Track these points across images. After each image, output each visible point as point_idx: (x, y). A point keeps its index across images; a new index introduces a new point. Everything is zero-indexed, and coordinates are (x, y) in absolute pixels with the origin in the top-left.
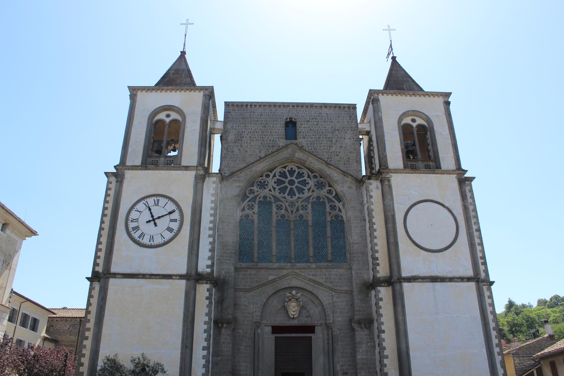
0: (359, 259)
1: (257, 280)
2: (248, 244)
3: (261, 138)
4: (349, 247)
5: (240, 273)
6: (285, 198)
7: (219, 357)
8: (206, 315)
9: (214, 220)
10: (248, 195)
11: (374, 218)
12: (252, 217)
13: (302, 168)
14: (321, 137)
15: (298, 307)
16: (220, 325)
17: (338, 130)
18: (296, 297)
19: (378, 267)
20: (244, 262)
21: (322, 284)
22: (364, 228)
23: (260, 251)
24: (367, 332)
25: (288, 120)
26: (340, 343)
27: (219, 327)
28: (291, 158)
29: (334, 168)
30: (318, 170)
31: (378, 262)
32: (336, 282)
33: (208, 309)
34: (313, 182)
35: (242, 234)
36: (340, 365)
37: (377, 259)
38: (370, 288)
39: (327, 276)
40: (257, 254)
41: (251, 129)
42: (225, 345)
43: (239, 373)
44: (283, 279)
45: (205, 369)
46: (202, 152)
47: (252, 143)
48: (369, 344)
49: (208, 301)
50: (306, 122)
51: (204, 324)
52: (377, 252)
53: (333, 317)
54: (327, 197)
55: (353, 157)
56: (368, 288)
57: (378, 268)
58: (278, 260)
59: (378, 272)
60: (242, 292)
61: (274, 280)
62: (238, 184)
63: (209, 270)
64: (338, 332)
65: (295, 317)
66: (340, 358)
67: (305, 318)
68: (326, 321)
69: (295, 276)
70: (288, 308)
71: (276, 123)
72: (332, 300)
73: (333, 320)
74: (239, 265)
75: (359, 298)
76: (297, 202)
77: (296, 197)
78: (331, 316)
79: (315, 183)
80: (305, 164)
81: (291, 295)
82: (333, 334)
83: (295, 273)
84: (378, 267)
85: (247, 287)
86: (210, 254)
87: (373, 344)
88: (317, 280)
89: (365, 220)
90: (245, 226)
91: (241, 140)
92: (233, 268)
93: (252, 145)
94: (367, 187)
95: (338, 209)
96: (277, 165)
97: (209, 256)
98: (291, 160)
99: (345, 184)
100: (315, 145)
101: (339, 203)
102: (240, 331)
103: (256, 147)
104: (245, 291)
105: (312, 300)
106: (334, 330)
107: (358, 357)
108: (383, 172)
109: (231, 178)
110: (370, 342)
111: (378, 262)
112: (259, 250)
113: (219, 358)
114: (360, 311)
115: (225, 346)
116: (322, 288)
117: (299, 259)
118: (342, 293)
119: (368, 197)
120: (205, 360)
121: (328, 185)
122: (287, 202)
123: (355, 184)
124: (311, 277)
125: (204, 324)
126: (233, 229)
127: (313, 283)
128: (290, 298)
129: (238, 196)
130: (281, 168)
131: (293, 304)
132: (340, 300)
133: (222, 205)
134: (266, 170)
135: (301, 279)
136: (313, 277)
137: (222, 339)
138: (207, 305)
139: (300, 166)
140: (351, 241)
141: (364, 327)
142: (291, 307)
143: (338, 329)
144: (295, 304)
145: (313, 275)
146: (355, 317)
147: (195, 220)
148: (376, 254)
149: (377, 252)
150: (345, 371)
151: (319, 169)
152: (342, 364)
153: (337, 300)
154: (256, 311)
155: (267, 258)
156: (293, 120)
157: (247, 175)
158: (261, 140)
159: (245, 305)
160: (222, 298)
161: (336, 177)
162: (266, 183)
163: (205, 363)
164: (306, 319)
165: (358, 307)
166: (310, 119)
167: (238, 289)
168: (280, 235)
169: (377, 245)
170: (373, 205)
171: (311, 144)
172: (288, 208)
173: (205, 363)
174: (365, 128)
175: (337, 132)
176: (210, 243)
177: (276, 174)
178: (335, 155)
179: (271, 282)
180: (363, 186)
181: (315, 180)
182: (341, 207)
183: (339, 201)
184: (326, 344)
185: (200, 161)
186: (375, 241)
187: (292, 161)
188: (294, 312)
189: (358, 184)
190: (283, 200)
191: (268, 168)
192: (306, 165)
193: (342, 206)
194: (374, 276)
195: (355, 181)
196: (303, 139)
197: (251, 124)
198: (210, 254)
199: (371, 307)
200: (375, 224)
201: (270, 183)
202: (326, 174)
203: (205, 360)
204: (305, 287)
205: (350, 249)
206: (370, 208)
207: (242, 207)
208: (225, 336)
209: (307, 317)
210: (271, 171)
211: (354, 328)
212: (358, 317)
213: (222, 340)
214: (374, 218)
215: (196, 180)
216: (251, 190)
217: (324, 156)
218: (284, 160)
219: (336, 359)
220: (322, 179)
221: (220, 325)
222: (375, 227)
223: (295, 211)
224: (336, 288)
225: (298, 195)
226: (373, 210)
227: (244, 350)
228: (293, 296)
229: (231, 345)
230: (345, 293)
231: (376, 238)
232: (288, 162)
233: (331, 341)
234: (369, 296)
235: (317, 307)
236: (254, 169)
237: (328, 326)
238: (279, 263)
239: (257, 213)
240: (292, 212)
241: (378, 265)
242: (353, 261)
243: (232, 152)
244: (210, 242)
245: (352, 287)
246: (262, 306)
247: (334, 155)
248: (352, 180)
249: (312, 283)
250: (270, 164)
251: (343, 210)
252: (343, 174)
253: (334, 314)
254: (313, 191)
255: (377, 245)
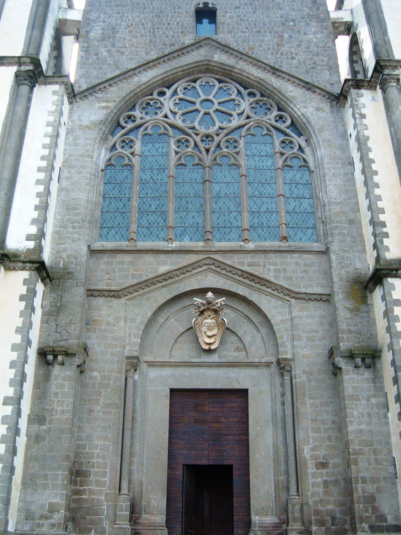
0: (344, 233)
1: (135, 273)
2: (120, 208)
3: (150, 32)
4: (321, 212)
5: (101, 261)
6: (193, 128)
7: (44, 425)
8: (16, 332)
9: (49, 154)
10: (124, 125)
11: (371, 151)
12: (129, 159)
13: (227, 82)
14: (262, 31)
15: (219, 329)
16: (50, 358)
17: (293, 21)
18: (214, 305)
19: (385, 240)
20: (109, 241)
21: (269, 282)
22: (350, 176)
23: (143, 221)
24: (367, 374)
25: (201, 6)
26: (308, 402)
27: (48, 364)
28: (206, 62)
29: (287, 77)
30: (256, 81)
31: (384, 230)
32: (296, 278)
33: (22, 319)
34: (248, 103)
35: (108, 191)
36: (310, 446)
37: (383, 224)
38: (370, 286)
39: (278, 267)
40: (136, 226)
41: (133, 20)
42: (59, 399)
43: (89, 462)
44: (188, 274)
45: (4, 445)
46: (33, 38)
47: (134, 40)
48: (373, 400)
49: (23, 303)
50: (246, 264)
51: (12, 350)
52: (382, 211)
53: (293, 347)
54: (277, 129)
55: (323, 61)
56: (366, 287)
57: (386, 242)
58: (178, 237)
59: (387, 249)
60: (103, 298)
61: (169, 275)
62: (104, 104)
63: (31, 244)
64: (304, 378)
65: (213, 347)
66: (310, 433)
67: (234, 351)
68: (278, 354)
69: (213, 267)
70: (198, 329)
71: (178, 11)
72: (291, 313)
73: (293, 354)
74: (98, 245)
75: (348, 306)
76: (218, 135)
77: (217, 127)
78: (289, 346)
79: (252, 104)
80: (232, 73)
81: (204, 302)
82: (294, 382)
83: (213, 261)
84: (385, 240)
85: (113, 288)
86: (35, 214)
87: (382, 400)
88: (257, 274)
89: (352, 164)
90: (114, 177)
91: (114, 37)
92: (85, 249)
93: (133, 44)
94: (354, 100)
95: (297, 147)
96: (179, 74)
97: (34, 219)
98: (206, 67)
99: (309, 104)
100: (251, 43)
101: (299, 137)
102: (95, 374)
103: (140, 46)
104: (109, 296)
105: (248, 315)
106: (295, 375)
107: (350, 428)
108: (385, 66)
109: (91, 94)
110: (375, 396)
111: (384, 230)
112: (142, 218)
113: (44, 427)
114: (350, 332)
115: (58, 401)
116: (269, 290)
117: (221, 233)
118: (310, 299)
119: (357, 116)
120: (7, 426)
121: (276, 108)
122: (197, 134)
123: (329, 104)
124: (245, 268)
125: (12, 350)
126: (90, 179)
127: (250, 281)
128: (203, 308)
129: (102, 122)
130: (188, 81)
131: (209, 321)
132: (305, 313)
133: (71, 138)
134: (158, 83)
135: (224, 272)
136: (250, 268)
137: (54, 387)
138: (21, 311)
139: (222, 78)
140: (326, 200)
141: (360, 364)
142: (204, 329)
143: (304, 372)
144: (213, 321)
145: (250, 265)
146: (341, 344)
147: (8, 145)
148: (380, 215)
149: (382, 211)
150: (322, 460)
151: (258, 80)
152: (315, 446)
153: (300, 314)
154: (130, 334)
155: (155, 233)
156: (210, 6)
157: (122, 89)
158: (150, 36)
159: (108, 323)
160: (59, 304)
161: (291, 92)
162: (159, 105)
163: (5, 433)
164: (237, 354)
165: (345, 324)
166: (240, 4)
167: (95, 290)
168: (182, 189)
169: (381, 200)
170: (367, 129)
171: (244, 41)
172: (200, 144)
173: (5, 433)
174: (342, 18)
175: (292, 24)
176: (38, 195)
177: (179, 91)
178: (290, 58)
179: (163, 277)
180: (344, 107)
181: (252, 100)
182: (303, 144)
183: (300, 134)
184: (279, 405)
185: (28, 51)
186: (377, 192)
187: (207, 69)
188: (210, 337)
189: (334, 103)
190: (190, 131)
191: (163, 78)
192: (234, 74)
193: (304, 142)
194: (378, 259)
195: (329, 98)
196: (229, 34)
197: (133, 12)
198: (35, 214)
199: (372, 323)
200: (375, 163)
201: (166, 105)
202: (273, 87)
203: (7, 426)
204: (234, 290)
205: (325, 216)
206: (361, 134)
207: (111, 143)
208: (60, 382)
209: (237, 349)
210: (169, 87)
211: (340, 366)
212: (346, 343)
213: (53, 389)
214: (371, 151)
215: (16, 80)
216: (129, 117)
217: (267, 59)
218: (192, 66)
219: (300, 435)
220: (265, 99)
221: (50, 358)
222: (374, 167)
223: (212, 149)
224: (298, 290)
225: (219, 124)
226: (368, 138)
227: (101, 414)
228: (209, 303)
229: (71, 400)
230: (316, 299)
231: (377, 186)
232: (201, 72)
233: (289, 398)
234: (369, 302)
235: (259, 330)
236: (136, 79)
237: (282, 366)
238: (180, 241)
239: (140, 154)
240: (207, 151)
241: (387, 235)
242: (332, 236)
243: (97, 54)
244: (37, 193)
245: (332, 287)
246: (144, 326)
247: (288, 58)
248: (322, 96)
249: (247, 281)
250: (166, 72)
251: (307, 150)
252: (305, 87)
253: (295, 343)
254: (248, 117)
255: (381, 200)
